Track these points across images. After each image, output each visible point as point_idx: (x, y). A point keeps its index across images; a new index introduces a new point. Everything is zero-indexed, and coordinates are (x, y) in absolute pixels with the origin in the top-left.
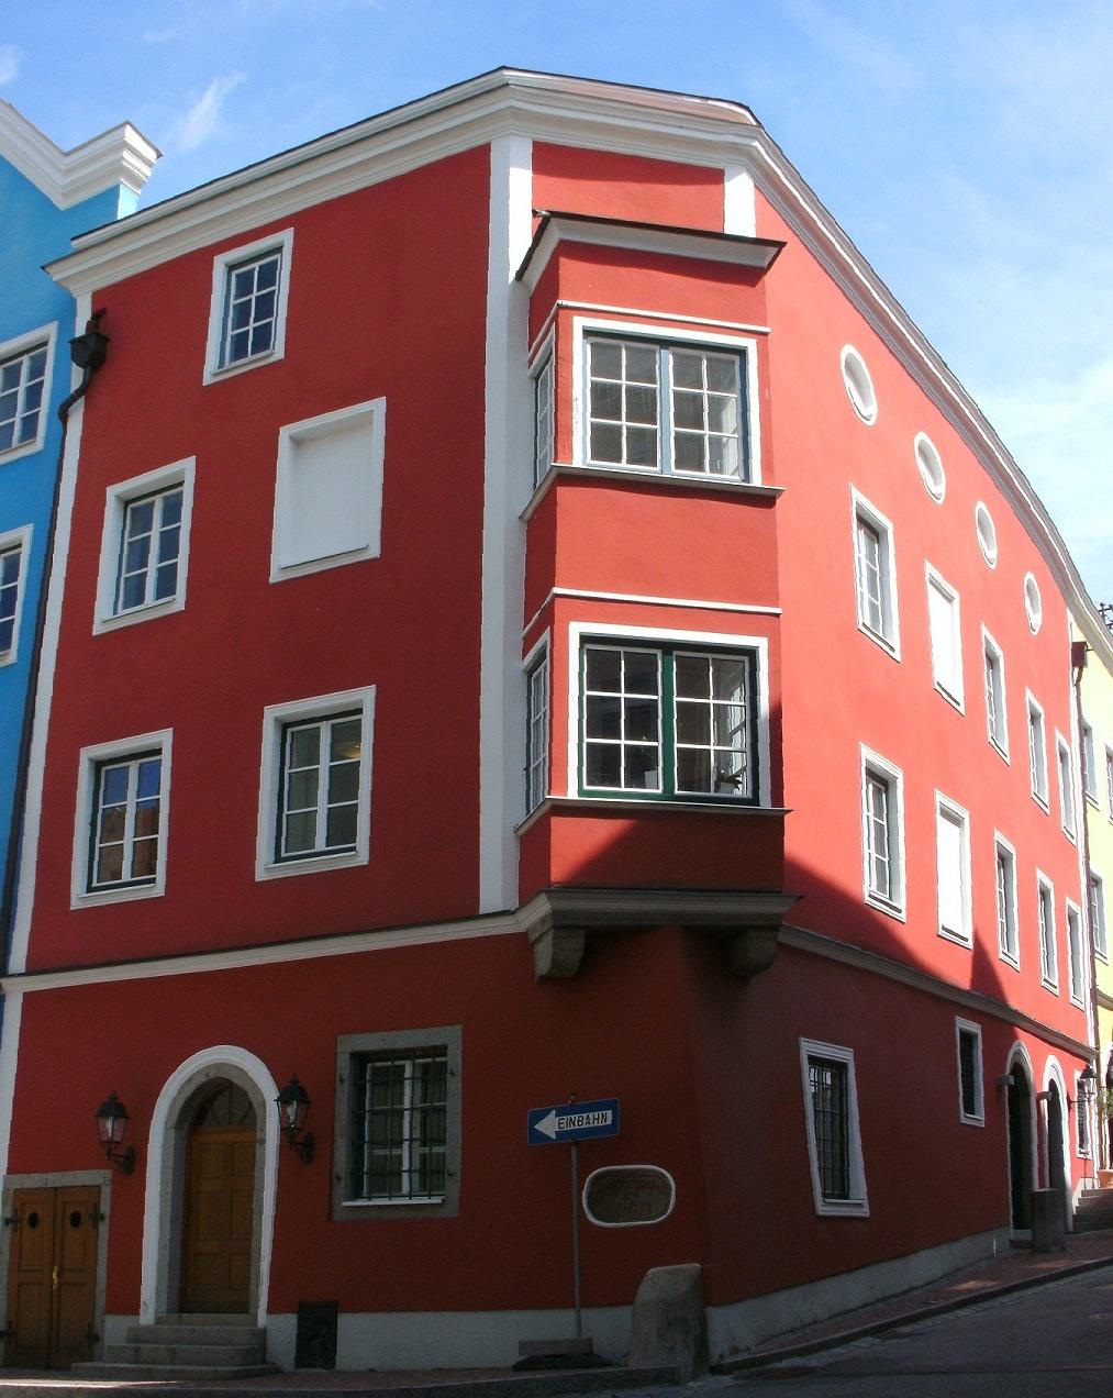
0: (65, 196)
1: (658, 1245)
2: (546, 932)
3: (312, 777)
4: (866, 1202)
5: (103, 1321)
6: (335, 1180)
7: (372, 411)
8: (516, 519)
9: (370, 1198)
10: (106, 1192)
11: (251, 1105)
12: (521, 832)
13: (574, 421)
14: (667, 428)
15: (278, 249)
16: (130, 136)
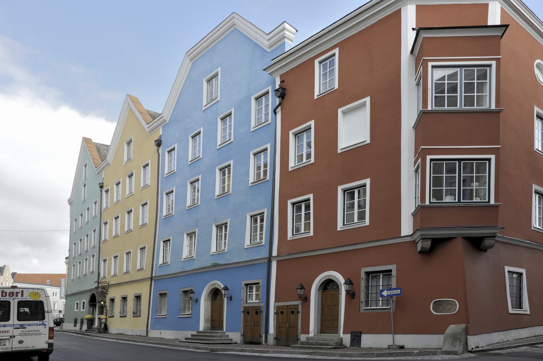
0: (269, 48)
1: (453, 319)
2: (420, 240)
3: (353, 204)
4: (528, 310)
5: (300, 335)
6: (361, 303)
7: (366, 101)
8: (412, 129)
9: (371, 307)
10: (300, 307)
11: (338, 286)
12: (413, 214)
13: (428, 96)
14: (461, 94)
15: (334, 55)
16: (286, 25)
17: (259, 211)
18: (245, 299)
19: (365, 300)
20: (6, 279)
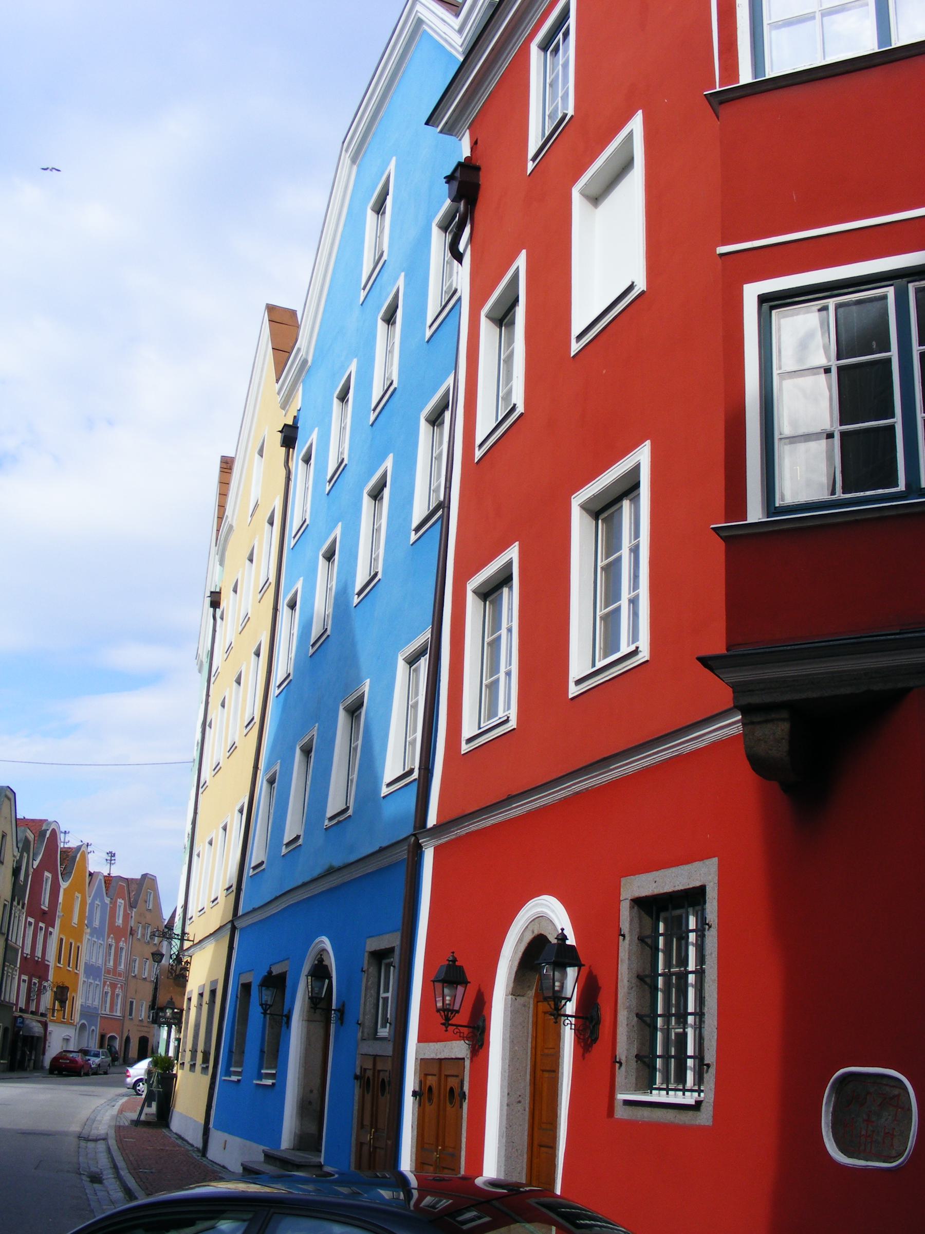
17: (923, 466)
18: (368, 1022)
19: (634, 1052)
20: (145, 917)
